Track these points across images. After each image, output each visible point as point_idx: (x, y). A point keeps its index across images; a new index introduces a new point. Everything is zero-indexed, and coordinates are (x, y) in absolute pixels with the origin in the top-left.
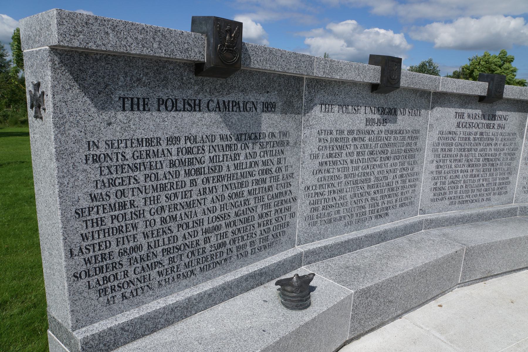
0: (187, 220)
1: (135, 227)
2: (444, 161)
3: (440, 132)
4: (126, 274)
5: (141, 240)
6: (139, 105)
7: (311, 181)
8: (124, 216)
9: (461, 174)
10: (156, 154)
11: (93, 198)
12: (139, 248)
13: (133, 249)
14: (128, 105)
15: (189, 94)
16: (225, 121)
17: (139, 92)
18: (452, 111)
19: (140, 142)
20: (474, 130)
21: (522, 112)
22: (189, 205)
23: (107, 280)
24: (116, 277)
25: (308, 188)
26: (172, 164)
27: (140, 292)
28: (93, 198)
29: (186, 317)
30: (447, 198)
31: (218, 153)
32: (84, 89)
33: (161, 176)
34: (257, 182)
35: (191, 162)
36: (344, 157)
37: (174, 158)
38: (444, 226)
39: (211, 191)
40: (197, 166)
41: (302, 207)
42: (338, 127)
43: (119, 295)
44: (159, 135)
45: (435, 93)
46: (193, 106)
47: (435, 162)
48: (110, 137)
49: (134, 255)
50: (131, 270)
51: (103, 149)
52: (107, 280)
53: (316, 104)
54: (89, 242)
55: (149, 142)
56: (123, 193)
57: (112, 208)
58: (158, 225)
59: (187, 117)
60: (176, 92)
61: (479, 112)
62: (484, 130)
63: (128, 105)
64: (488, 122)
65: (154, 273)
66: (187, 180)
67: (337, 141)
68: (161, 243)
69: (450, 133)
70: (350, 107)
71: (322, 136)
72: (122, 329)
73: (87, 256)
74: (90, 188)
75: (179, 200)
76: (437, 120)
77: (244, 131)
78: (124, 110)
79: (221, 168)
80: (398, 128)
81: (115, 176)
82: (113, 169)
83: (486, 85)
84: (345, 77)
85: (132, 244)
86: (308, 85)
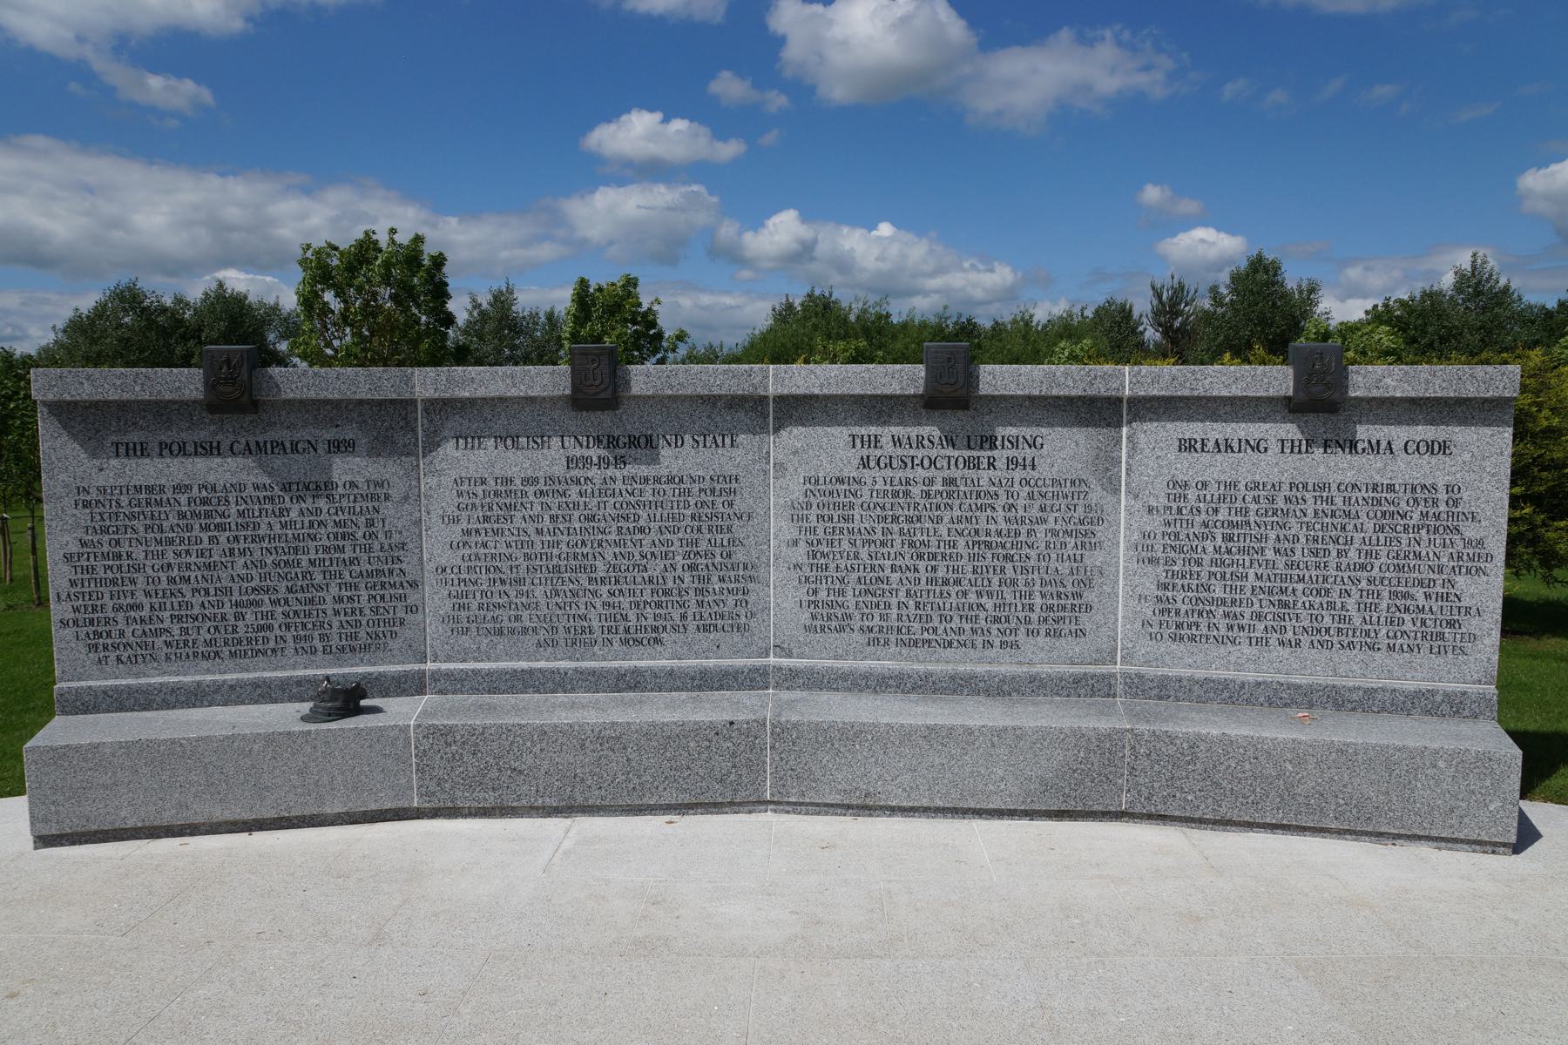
0: (205, 585)
1: (133, 582)
2: (831, 543)
3: (808, 480)
4: (122, 633)
5: (140, 597)
6: (138, 450)
7: (449, 558)
8: (120, 568)
9: (896, 576)
10: (159, 503)
11: (83, 544)
12: (139, 607)
13: (131, 607)
14: (122, 450)
15: (203, 435)
16: (260, 466)
17: (135, 437)
18: (841, 434)
19: (138, 489)
20: (920, 473)
21: (1095, 425)
22: (208, 567)
23: (99, 635)
24: (109, 634)
25: (444, 570)
26: (182, 515)
27: (140, 659)
28: (83, 544)
29: (194, 706)
30: (856, 628)
31: (250, 506)
32: (74, 436)
33: (706, 615)
34: (326, 550)
35: (208, 515)
36: (518, 522)
37: (184, 509)
38: (837, 689)
39: (243, 553)
40: (218, 520)
41: (435, 600)
42: (498, 472)
43: (113, 656)
44: (163, 482)
45: (781, 399)
46: (209, 449)
47: (802, 543)
48: (101, 483)
49: (132, 613)
50: (128, 633)
51: (94, 495)
52: (99, 635)
53: (446, 438)
54: (78, 589)
55: (150, 489)
56: (118, 542)
57: (105, 556)
58: (164, 584)
59: (200, 463)
60: (183, 435)
61: (931, 431)
62: (955, 473)
63: (122, 450)
64: (967, 453)
65: (159, 642)
66: (205, 536)
67: (504, 498)
68: (168, 606)
69: (840, 480)
70: (523, 440)
71: (465, 487)
72: (105, 692)
73: (76, 604)
74: (80, 534)
75: (193, 559)
76: (795, 453)
77: (295, 478)
78: (118, 456)
79: (256, 526)
80: (665, 472)
81: (108, 523)
82: (106, 516)
83: (920, 370)
84: (481, 392)
85: (129, 600)
86: (426, 410)
